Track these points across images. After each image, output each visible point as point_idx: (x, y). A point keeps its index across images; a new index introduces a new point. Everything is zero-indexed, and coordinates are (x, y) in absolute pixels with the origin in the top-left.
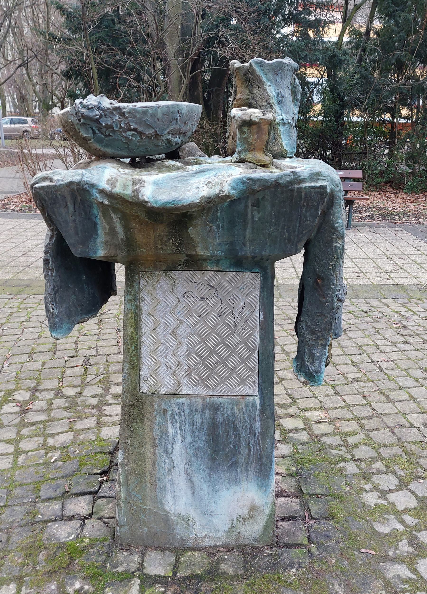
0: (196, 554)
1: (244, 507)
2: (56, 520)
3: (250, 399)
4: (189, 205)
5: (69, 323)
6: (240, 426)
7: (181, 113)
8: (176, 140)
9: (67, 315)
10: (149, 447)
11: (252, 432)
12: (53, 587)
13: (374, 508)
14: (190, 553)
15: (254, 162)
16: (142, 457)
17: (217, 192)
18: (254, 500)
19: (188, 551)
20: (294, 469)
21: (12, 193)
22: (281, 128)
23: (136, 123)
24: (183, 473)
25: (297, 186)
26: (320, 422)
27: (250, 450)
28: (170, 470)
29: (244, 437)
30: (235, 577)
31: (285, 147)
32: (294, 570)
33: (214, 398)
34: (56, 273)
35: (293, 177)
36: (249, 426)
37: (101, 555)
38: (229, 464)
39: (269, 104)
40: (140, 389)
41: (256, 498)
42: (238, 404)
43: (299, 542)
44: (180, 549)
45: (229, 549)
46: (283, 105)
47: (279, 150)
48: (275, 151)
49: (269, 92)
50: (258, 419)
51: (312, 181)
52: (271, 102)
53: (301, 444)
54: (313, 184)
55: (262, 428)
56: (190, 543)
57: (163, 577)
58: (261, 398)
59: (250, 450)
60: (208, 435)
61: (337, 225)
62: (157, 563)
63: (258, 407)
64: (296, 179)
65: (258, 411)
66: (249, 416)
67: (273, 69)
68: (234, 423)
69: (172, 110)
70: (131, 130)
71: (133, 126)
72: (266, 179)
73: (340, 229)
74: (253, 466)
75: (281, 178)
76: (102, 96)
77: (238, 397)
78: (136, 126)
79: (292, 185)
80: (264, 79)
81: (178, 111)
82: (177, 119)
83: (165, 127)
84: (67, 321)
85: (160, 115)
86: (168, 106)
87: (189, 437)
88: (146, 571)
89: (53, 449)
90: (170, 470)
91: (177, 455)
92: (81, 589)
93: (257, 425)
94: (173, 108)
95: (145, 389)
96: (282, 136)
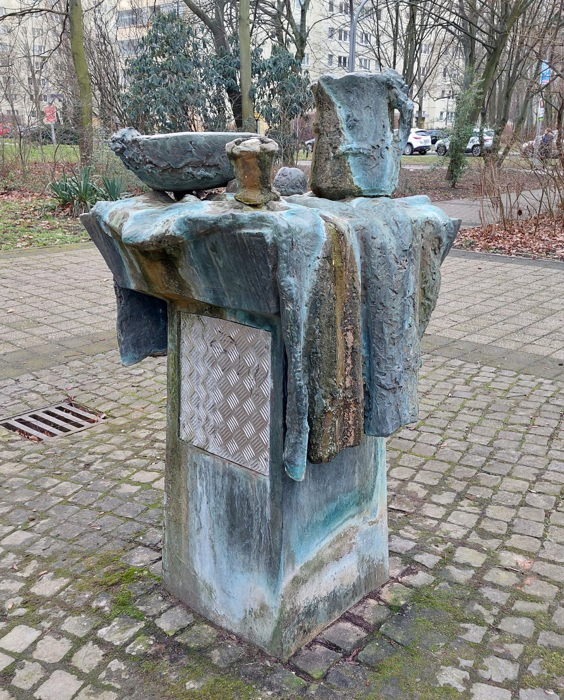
0: (211, 630)
1: (255, 600)
2: (148, 546)
3: (262, 478)
4: (143, 243)
5: (134, 352)
6: (252, 504)
7: (195, 145)
8: (199, 173)
9: (132, 345)
10: (184, 497)
11: (263, 517)
12: (87, 596)
13: (440, 687)
14: (206, 626)
15: (242, 200)
16: (179, 505)
17: (164, 231)
18: (264, 597)
19: (206, 623)
20: (402, 603)
21: (469, 225)
22: (350, 160)
23: (150, 156)
24: (208, 537)
25: (238, 232)
26: (506, 569)
27: (261, 538)
28: (198, 530)
29: (256, 520)
30: (215, 667)
31: (356, 183)
32: (270, 693)
33: (232, 465)
34: (126, 301)
35: (231, 220)
36: (260, 510)
37: (142, 589)
38: (244, 545)
39: (338, 129)
40: (179, 435)
41: (266, 596)
42: (251, 479)
43: (310, 672)
44: (201, 617)
45: (240, 640)
46: (355, 130)
47: (347, 187)
48: (341, 188)
49: (339, 115)
50: (268, 503)
51: (255, 227)
52: (340, 127)
53: (448, 581)
54: (251, 231)
55: (272, 516)
56: (211, 617)
57: (164, 633)
58: (271, 480)
59: (261, 538)
60: (227, 504)
61: (282, 284)
62: (172, 619)
63: (269, 490)
64: (234, 222)
65: (268, 496)
66: (261, 498)
67: (344, 87)
68: (247, 500)
69: (181, 141)
70: (147, 163)
71: (148, 158)
72: (204, 221)
73: (286, 289)
74: (264, 557)
75: (220, 221)
76: (130, 129)
77: (252, 472)
78: (151, 159)
79: (233, 230)
80: (334, 99)
81: (191, 143)
82: (191, 151)
83: (179, 160)
84: (133, 350)
85: (169, 148)
86: (176, 138)
87: (212, 500)
88: (157, 621)
89: (81, 462)
90: (198, 530)
91: (204, 515)
92: (103, 607)
93: (268, 511)
94: (183, 139)
95: (183, 436)
96: (352, 169)
